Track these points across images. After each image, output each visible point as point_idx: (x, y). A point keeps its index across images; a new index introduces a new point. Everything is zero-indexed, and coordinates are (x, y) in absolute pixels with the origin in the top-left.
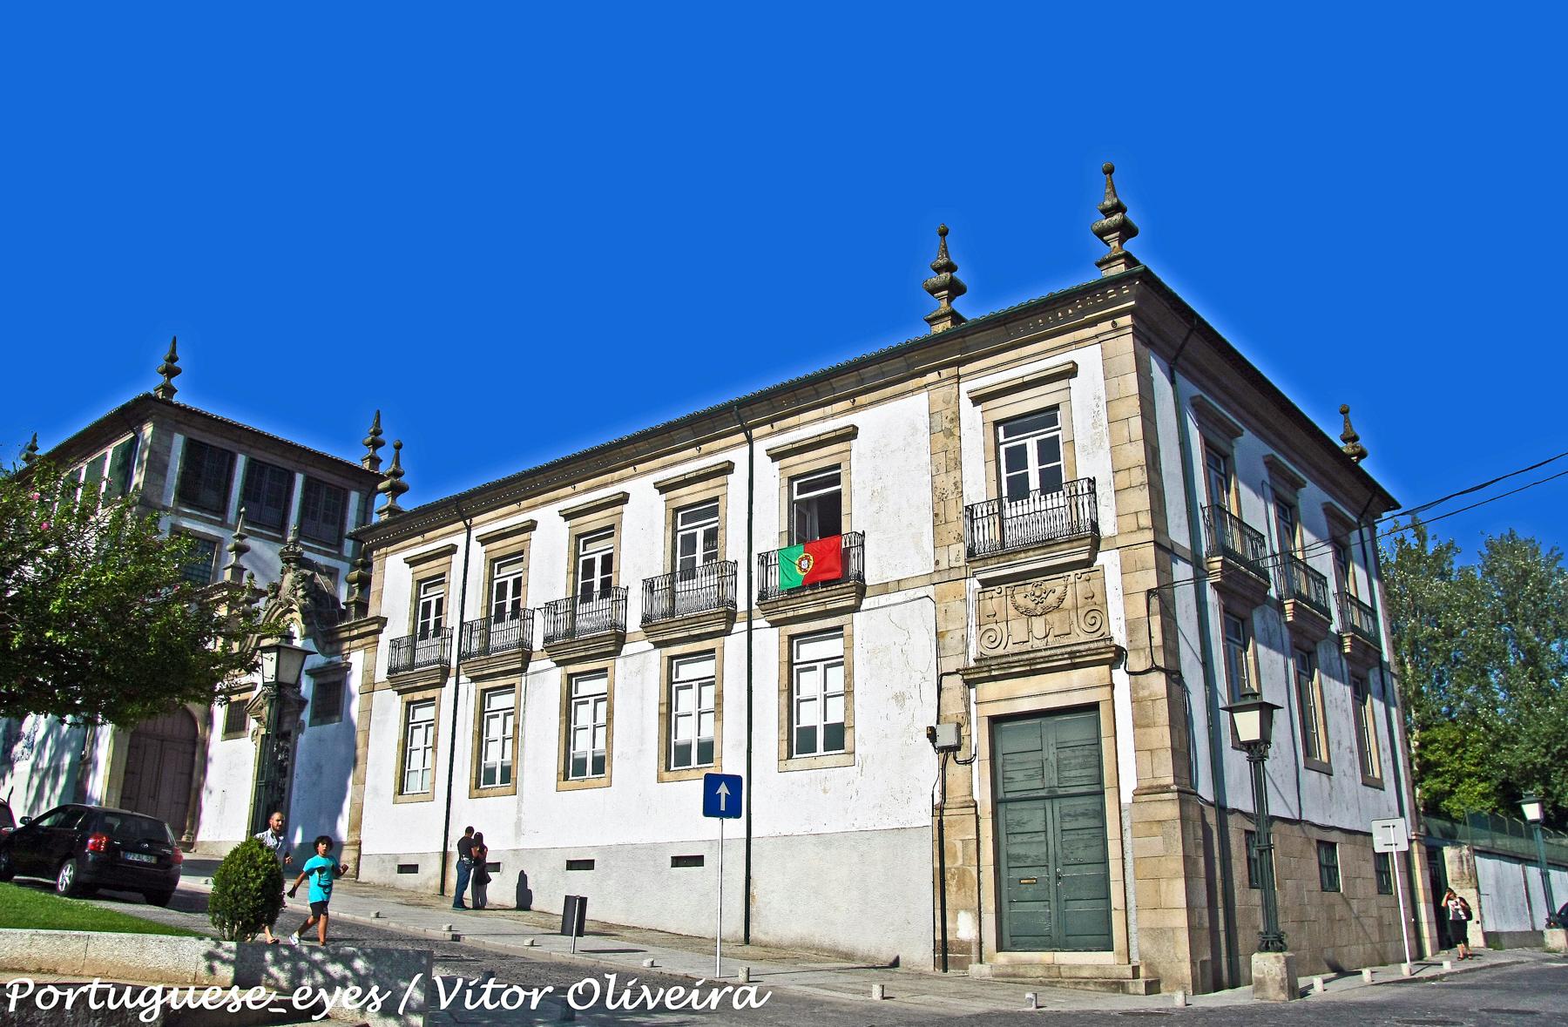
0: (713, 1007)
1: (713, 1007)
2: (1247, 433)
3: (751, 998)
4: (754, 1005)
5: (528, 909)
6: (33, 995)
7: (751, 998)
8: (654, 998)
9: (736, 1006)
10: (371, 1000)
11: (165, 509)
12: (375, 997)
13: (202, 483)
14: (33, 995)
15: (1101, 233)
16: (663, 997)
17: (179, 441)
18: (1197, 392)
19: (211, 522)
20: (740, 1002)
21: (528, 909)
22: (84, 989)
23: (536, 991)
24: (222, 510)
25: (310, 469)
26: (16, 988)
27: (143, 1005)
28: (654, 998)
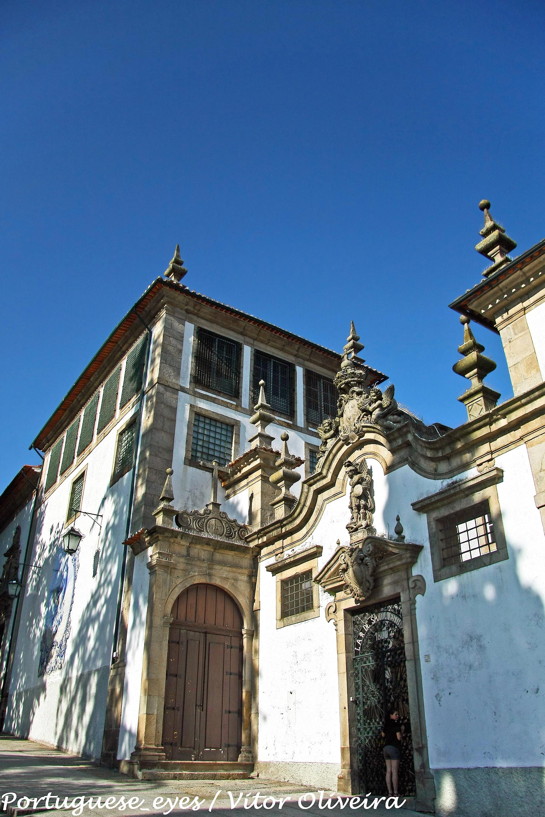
0: (375, 808)
1: (375, 808)
2: (484, 413)
3: (395, 803)
4: (397, 807)
5: (27, 739)
6: (18, 799)
7: (395, 803)
8: (173, 803)
9: (387, 807)
10: (121, 804)
11: (183, 390)
12: (123, 803)
13: (215, 367)
14: (18, 799)
15: (484, 251)
16: (178, 802)
17: (189, 331)
18: (118, 411)
19: (226, 405)
20: (389, 806)
21: (27, 739)
22: (43, 798)
23: (36, 799)
24: (236, 394)
25: (308, 364)
26: (7, 798)
27: (74, 806)
28: (173, 803)
